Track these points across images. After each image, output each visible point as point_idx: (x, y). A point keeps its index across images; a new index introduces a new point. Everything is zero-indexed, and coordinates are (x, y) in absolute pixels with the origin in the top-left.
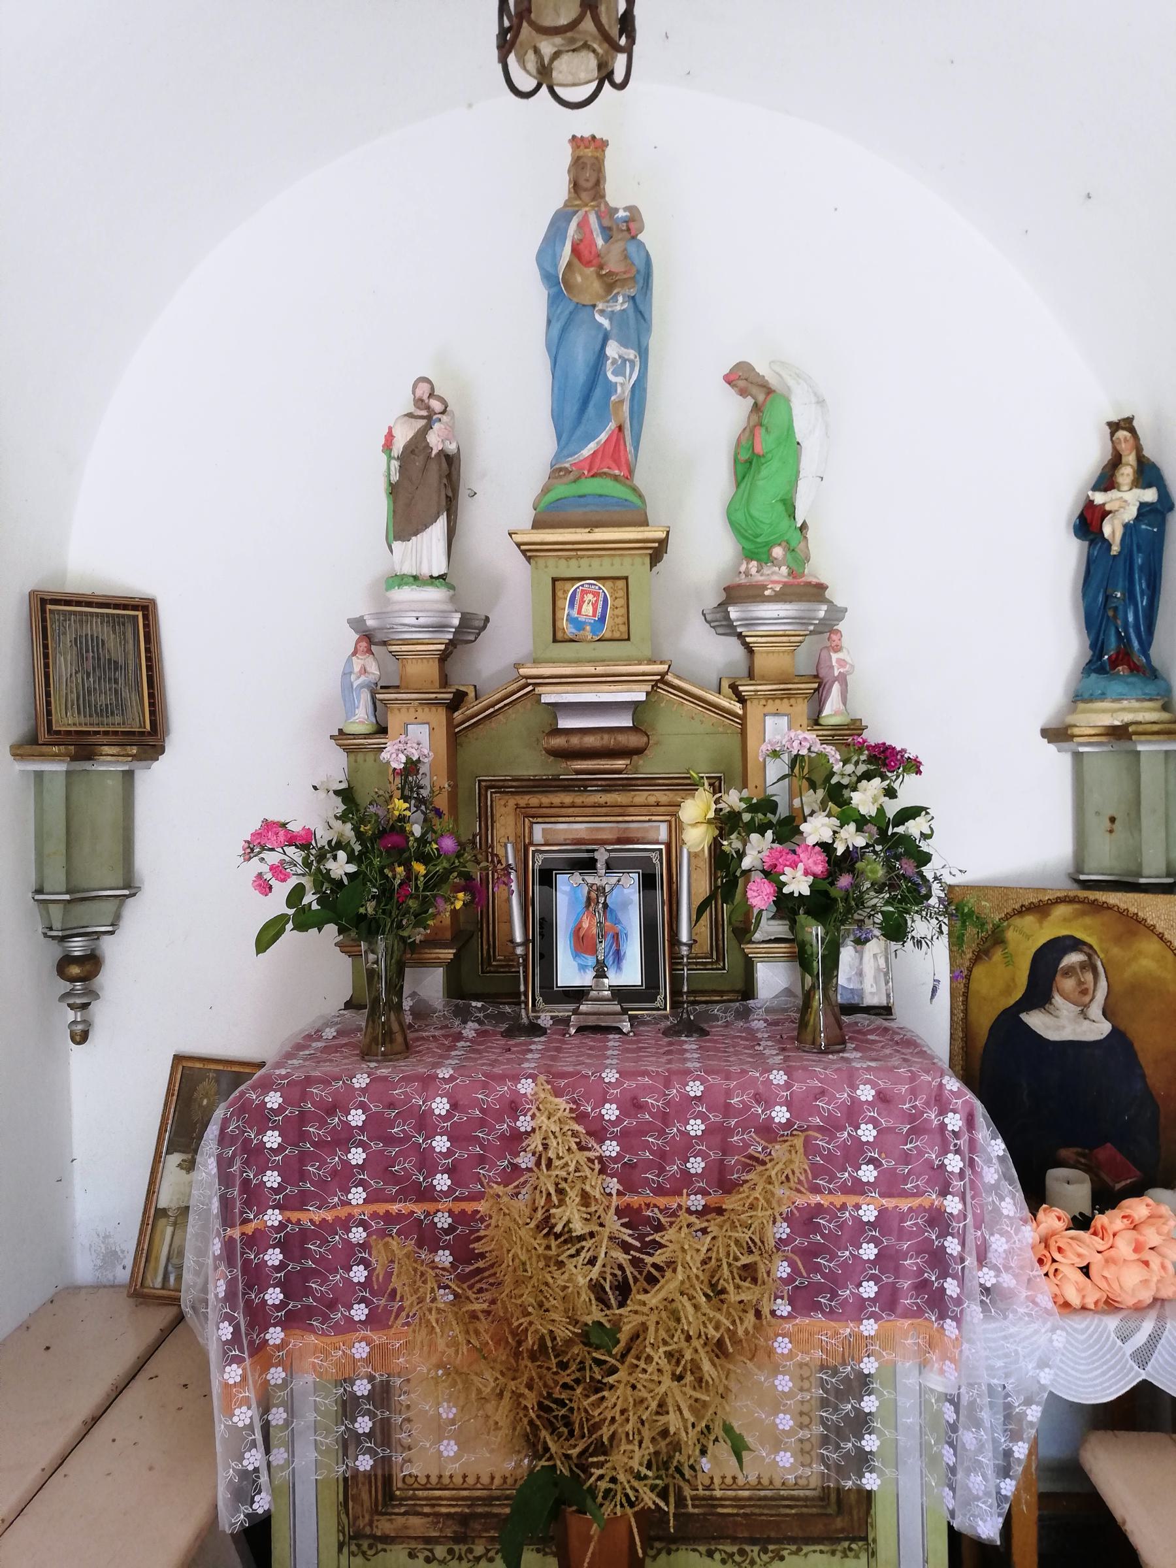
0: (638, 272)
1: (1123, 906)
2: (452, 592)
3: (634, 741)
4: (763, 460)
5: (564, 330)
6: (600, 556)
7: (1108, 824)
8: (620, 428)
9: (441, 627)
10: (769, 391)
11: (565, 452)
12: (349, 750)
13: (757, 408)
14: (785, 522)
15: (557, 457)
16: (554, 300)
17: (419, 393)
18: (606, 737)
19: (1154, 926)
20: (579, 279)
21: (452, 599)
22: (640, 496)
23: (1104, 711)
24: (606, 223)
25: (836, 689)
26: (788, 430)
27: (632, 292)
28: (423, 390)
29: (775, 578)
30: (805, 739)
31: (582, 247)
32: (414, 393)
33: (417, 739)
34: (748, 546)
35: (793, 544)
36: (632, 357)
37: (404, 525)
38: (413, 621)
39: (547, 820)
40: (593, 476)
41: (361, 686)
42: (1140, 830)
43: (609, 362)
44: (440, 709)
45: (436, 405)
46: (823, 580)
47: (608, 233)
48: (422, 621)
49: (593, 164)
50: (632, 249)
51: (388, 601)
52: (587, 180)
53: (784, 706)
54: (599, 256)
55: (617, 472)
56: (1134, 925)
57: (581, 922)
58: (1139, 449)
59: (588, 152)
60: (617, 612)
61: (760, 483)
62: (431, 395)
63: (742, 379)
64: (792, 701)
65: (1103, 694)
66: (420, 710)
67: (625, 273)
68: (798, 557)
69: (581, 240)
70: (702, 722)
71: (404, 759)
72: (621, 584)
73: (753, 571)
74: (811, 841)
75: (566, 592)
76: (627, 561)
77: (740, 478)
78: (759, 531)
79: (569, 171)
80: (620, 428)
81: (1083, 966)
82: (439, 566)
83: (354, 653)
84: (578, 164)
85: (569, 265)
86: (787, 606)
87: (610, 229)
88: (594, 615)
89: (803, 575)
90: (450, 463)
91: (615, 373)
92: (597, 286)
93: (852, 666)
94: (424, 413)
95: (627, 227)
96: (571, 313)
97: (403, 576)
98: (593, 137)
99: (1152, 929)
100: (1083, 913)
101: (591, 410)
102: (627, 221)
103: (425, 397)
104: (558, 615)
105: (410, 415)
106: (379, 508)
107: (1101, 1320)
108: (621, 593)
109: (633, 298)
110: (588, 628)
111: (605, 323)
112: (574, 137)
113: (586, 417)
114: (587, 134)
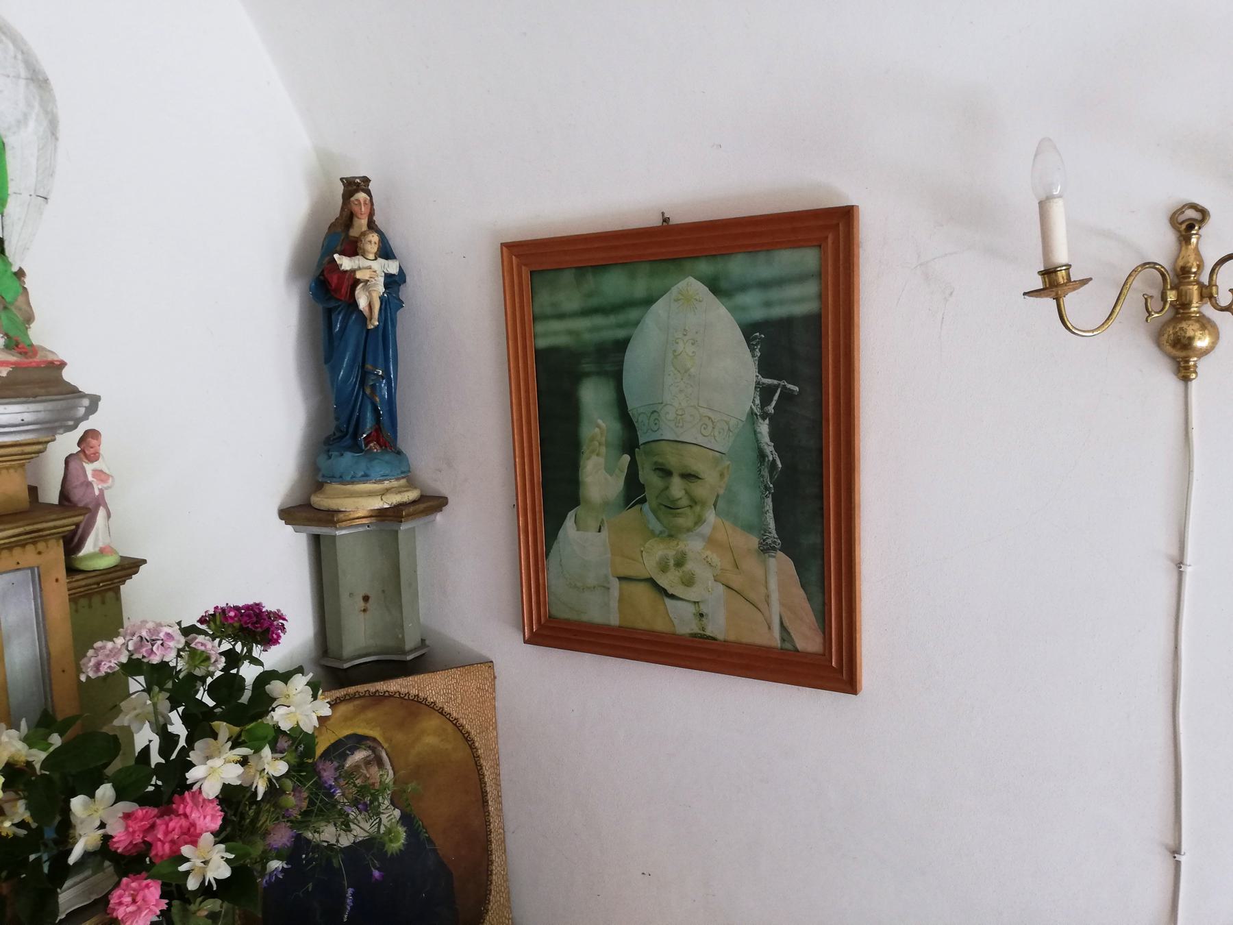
1: (403, 690)
7: (362, 604)
19: (434, 703)
23: (371, 494)
42: (401, 606)
56: (416, 706)
58: (371, 214)
64: (41, 546)
65: (366, 475)
74: (211, 790)
81: (367, 762)
86: (33, 407)
99: (432, 706)
100: (364, 708)
107: (95, 545)
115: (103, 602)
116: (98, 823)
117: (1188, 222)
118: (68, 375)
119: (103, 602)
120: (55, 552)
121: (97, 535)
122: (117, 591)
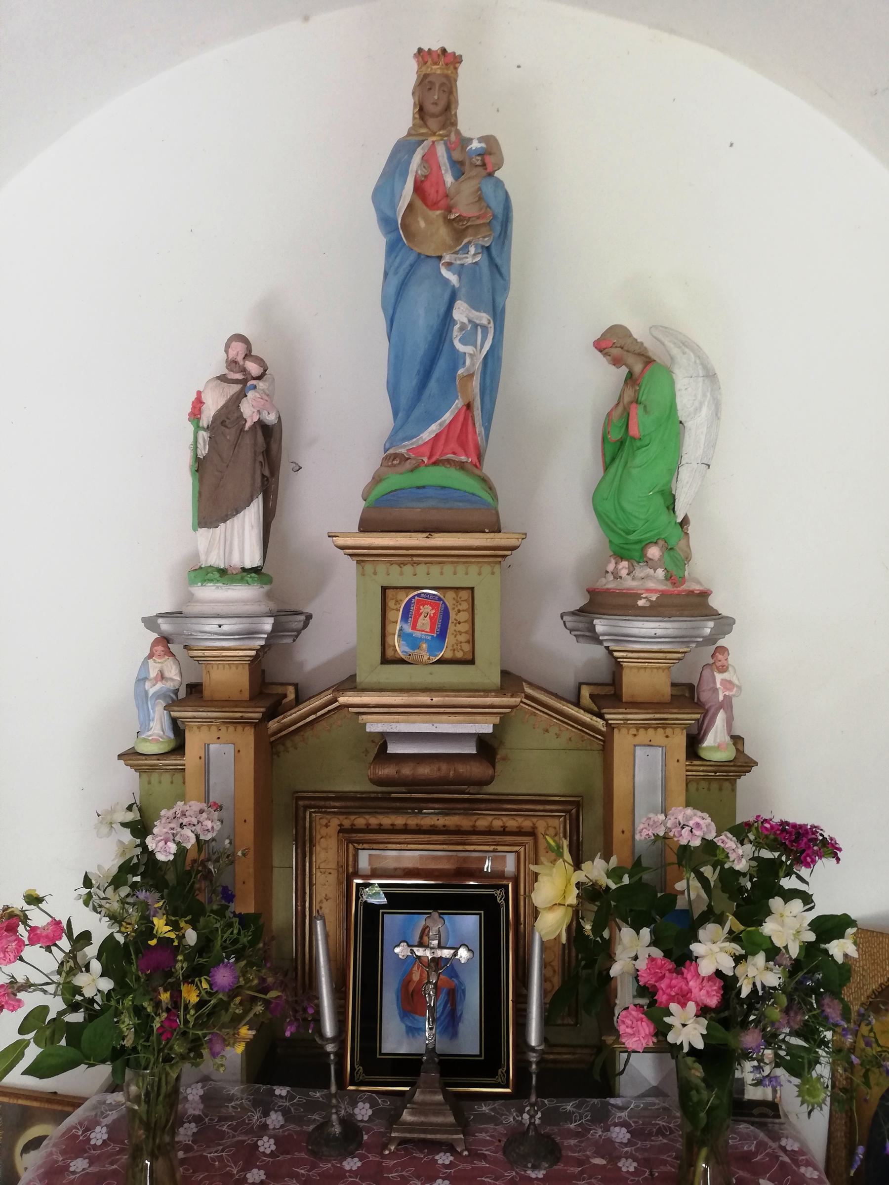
0: (494, 217)
2: (267, 587)
3: (477, 770)
4: (638, 443)
5: (403, 286)
6: (440, 563)
8: (469, 406)
9: (250, 634)
10: (648, 361)
11: (401, 435)
12: (139, 769)
13: (631, 379)
14: (664, 517)
15: (394, 438)
16: (392, 248)
17: (232, 353)
18: (444, 767)
20: (422, 224)
21: (269, 595)
22: (490, 488)
24: (457, 156)
25: (721, 717)
26: (671, 407)
27: (487, 242)
28: (238, 349)
29: (651, 585)
30: (698, 825)
31: (427, 186)
32: (226, 351)
33: (223, 755)
34: (617, 540)
35: (672, 542)
36: (484, 322)
37: (212, 509)
38: (215, 628)
39: (375, 846)
40: (435, 463)
41: (158, 696)
43: (457, 327)
44: (247, 728)
45: (253, 368)
46: (706, 586)
47: (458, 167)
48: (225, 628)
49: (443, 84)
50: (488, 188)
51: (190, 598)
52: (435, 104)
53: (658, 736)
54: (447, 196)
55: (463, 458)
57: (411, 973)
59: (437, 69)
60: (460, 628)
61: (635, 472)
62: (248, 355)
63: (614, 345)
64: (669, 731)
66: (223, 728)
67: (478, 218)
68: (678, 557)
69: (426, 177)
70: (558, 736)
71: (173, 848)
72: (465, 595)
73: (624, 573)
74: (706, 968)
75: (398, 602)
76: (473, 569)
77: (608, 460)
78: (631, 527)
79: (413, 94)
80: (469, 406)
82: (251, 557)
83: (151, 656)
84: (424, 84)
85: (410, 206)
87: (462, 163)
88: (432, 631)
89: (683, 580)
90: (268, 435)
91: (463, 341)
92: (443, 233)
93: (739, 688)
94: (239, 376)
95: (485, 160)
96: (412, 266)
97: (211, 569)
98: (444, 51)
101: (433, 384)
102: (482, 154)
103: (240, 359)
104: (389, 628)
105: (223, 378)
106: (182, 487)
107: (715, 741)
108: (465, 606)
109: (488, 249)
110: (424, 646)
111: (453, 278)
112: (420, 50)
113: (427, 392)
114: (435, 47)
115: (720, 789)
116: (633, 955)
117: (467, 574)
118: (714, 602)
119: (720, 789)
120: (680, 740)
121: (716, 732)
122: (733, 783)
